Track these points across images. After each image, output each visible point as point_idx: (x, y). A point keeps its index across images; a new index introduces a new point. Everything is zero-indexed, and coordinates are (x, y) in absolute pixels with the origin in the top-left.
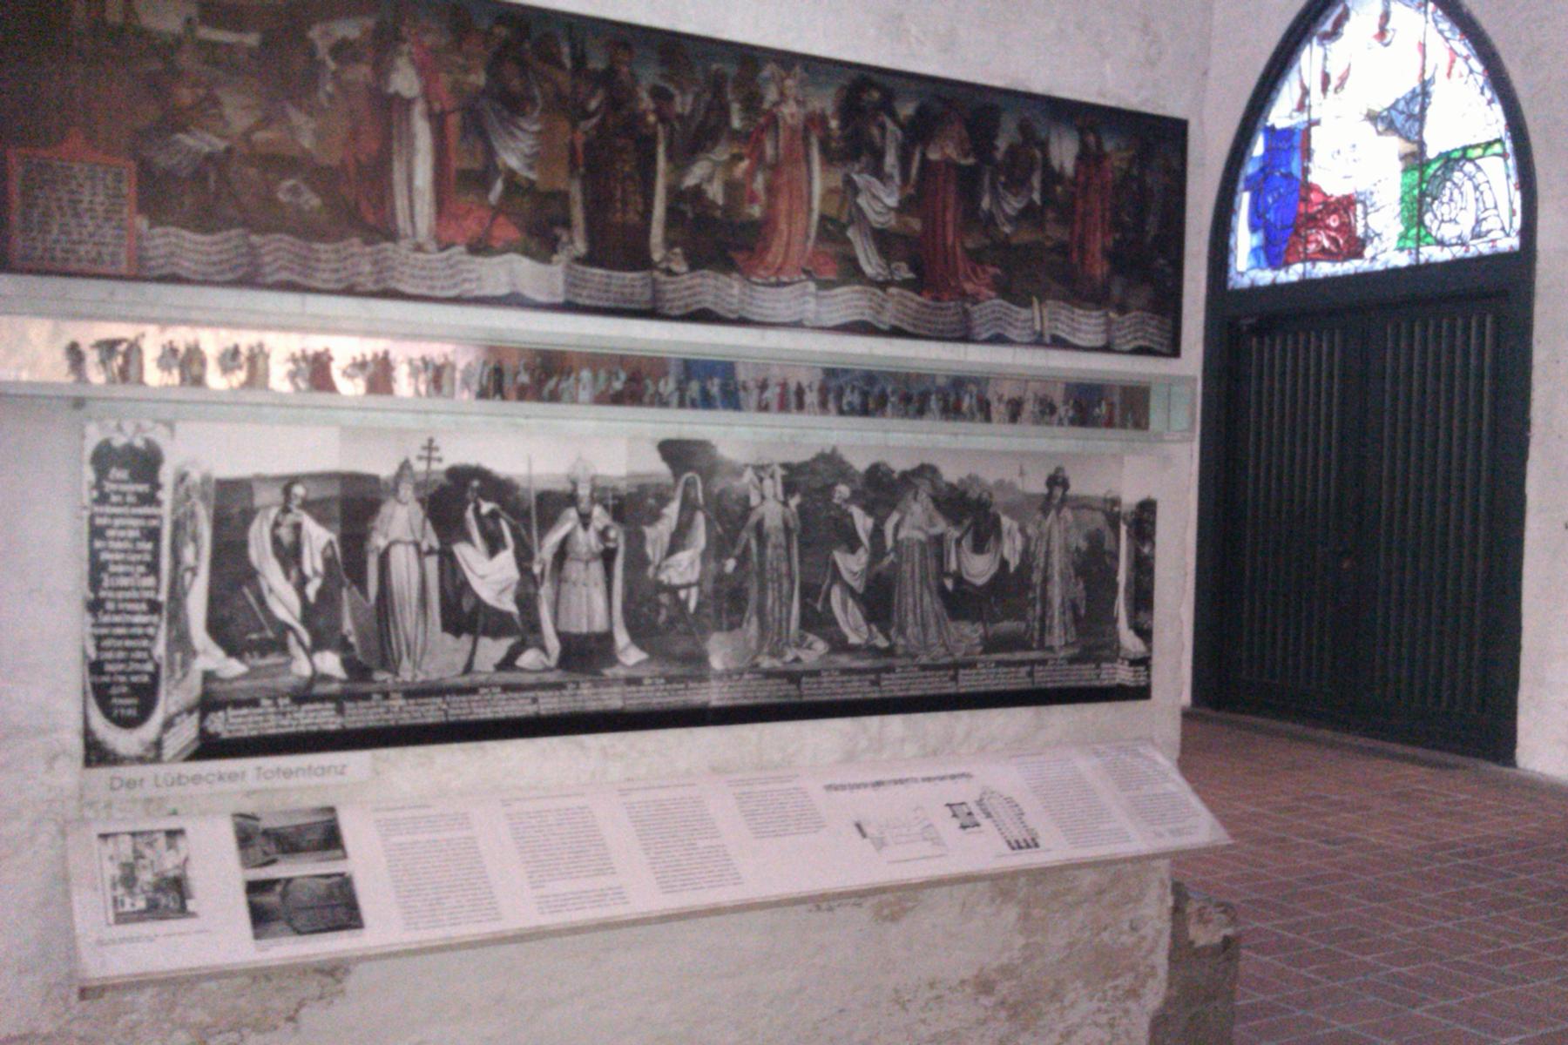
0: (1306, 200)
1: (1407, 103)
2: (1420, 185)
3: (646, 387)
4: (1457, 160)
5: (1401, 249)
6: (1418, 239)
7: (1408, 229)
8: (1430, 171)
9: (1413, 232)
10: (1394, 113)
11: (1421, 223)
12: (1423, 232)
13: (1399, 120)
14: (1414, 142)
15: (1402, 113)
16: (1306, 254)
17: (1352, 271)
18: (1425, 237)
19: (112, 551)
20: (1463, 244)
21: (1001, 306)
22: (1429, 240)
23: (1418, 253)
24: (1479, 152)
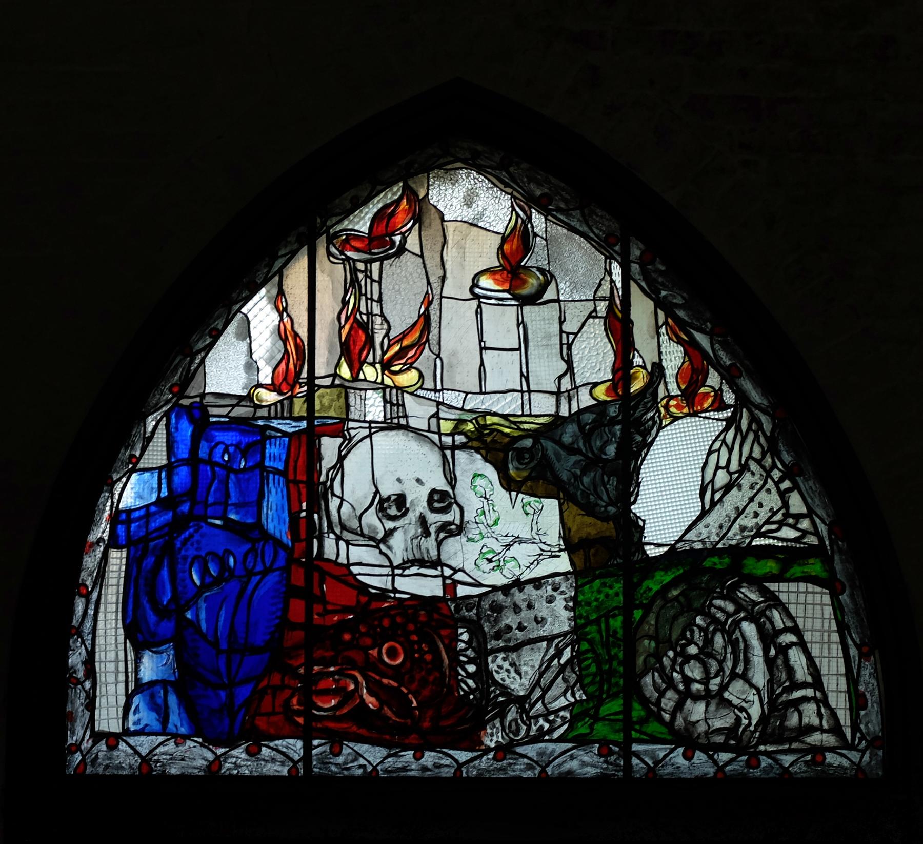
0: (311, 597)
1: (587, 435)
2: (627, 610)
3: (135, 527)
4: (719, 575)
5: (582, 742)
6: (627, 724)
7: (597, 698)
8: (654, 585)
9: (614, 706)
10: (549, 445)
11: (633, 690)
12: (637, 712)
13: (566, 466)
14: (605, 518)
15: (571, 450)
16: (309, 717)
17: (800, 696)
18: (643, 721)
19: (729, 461)
20: (739, 750)
21: (657, 539)
22: (653, 727)
23: (627, 754)
24: (770, 566)
